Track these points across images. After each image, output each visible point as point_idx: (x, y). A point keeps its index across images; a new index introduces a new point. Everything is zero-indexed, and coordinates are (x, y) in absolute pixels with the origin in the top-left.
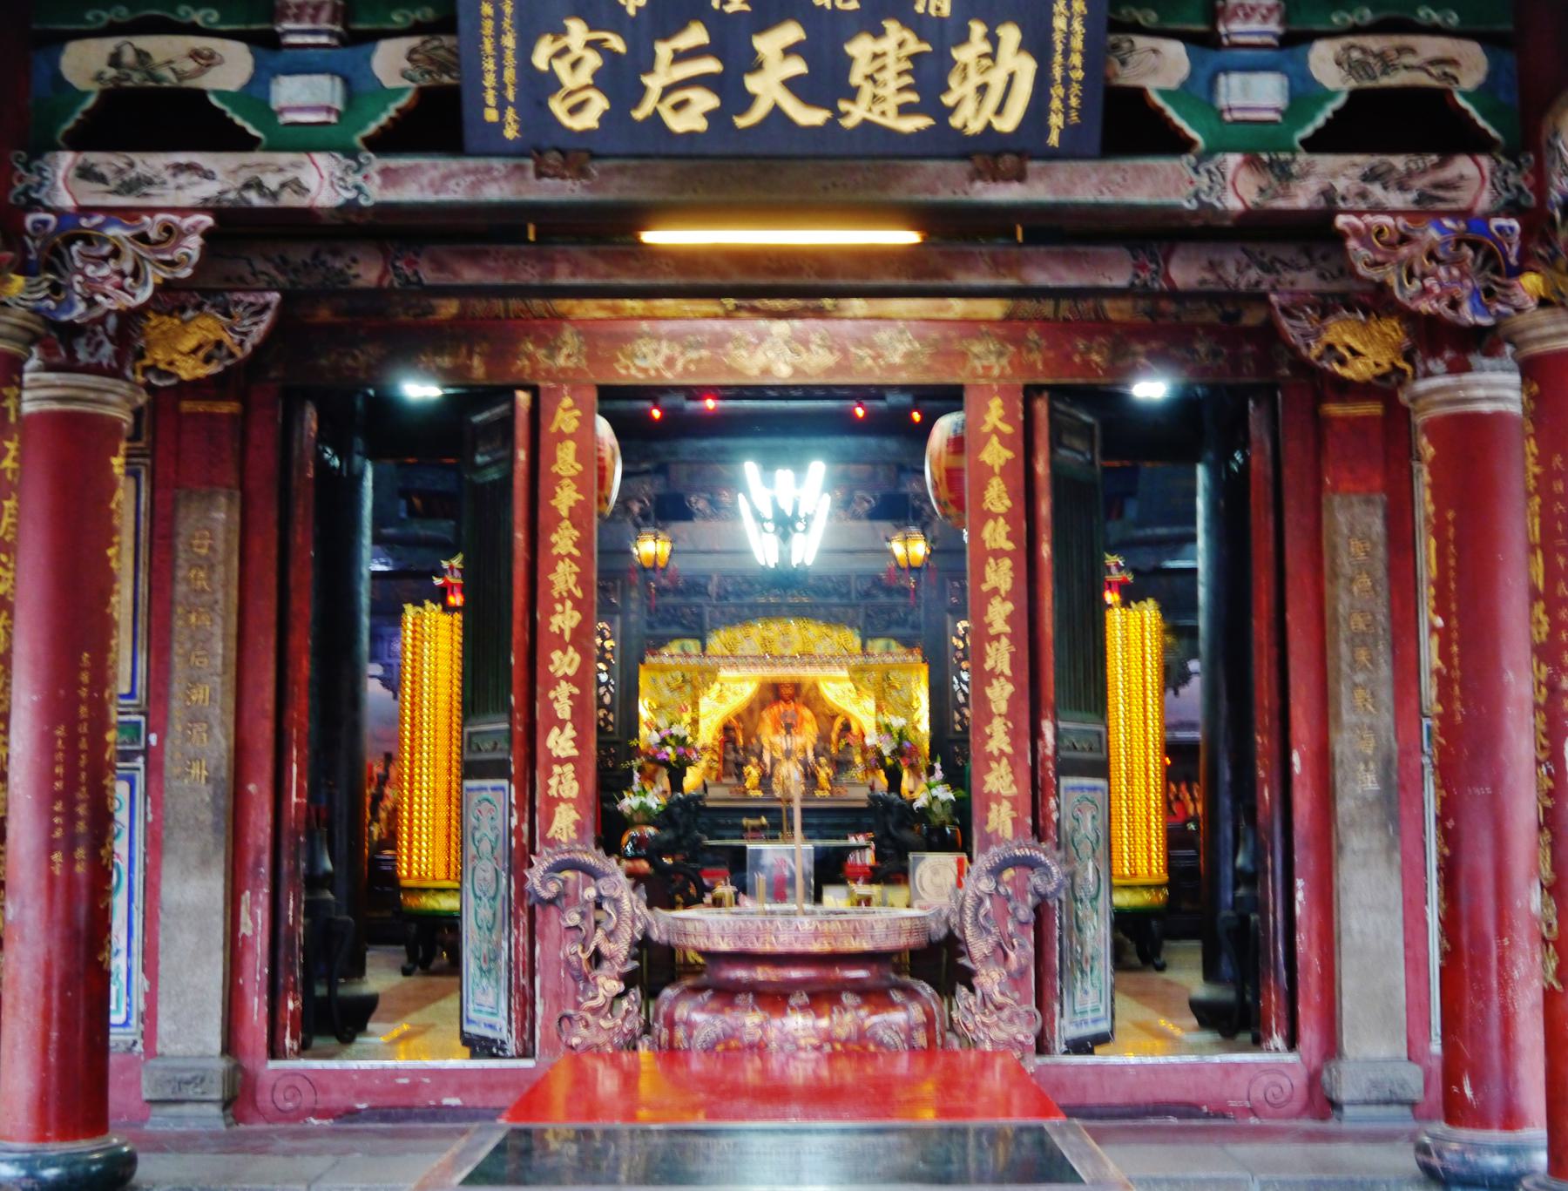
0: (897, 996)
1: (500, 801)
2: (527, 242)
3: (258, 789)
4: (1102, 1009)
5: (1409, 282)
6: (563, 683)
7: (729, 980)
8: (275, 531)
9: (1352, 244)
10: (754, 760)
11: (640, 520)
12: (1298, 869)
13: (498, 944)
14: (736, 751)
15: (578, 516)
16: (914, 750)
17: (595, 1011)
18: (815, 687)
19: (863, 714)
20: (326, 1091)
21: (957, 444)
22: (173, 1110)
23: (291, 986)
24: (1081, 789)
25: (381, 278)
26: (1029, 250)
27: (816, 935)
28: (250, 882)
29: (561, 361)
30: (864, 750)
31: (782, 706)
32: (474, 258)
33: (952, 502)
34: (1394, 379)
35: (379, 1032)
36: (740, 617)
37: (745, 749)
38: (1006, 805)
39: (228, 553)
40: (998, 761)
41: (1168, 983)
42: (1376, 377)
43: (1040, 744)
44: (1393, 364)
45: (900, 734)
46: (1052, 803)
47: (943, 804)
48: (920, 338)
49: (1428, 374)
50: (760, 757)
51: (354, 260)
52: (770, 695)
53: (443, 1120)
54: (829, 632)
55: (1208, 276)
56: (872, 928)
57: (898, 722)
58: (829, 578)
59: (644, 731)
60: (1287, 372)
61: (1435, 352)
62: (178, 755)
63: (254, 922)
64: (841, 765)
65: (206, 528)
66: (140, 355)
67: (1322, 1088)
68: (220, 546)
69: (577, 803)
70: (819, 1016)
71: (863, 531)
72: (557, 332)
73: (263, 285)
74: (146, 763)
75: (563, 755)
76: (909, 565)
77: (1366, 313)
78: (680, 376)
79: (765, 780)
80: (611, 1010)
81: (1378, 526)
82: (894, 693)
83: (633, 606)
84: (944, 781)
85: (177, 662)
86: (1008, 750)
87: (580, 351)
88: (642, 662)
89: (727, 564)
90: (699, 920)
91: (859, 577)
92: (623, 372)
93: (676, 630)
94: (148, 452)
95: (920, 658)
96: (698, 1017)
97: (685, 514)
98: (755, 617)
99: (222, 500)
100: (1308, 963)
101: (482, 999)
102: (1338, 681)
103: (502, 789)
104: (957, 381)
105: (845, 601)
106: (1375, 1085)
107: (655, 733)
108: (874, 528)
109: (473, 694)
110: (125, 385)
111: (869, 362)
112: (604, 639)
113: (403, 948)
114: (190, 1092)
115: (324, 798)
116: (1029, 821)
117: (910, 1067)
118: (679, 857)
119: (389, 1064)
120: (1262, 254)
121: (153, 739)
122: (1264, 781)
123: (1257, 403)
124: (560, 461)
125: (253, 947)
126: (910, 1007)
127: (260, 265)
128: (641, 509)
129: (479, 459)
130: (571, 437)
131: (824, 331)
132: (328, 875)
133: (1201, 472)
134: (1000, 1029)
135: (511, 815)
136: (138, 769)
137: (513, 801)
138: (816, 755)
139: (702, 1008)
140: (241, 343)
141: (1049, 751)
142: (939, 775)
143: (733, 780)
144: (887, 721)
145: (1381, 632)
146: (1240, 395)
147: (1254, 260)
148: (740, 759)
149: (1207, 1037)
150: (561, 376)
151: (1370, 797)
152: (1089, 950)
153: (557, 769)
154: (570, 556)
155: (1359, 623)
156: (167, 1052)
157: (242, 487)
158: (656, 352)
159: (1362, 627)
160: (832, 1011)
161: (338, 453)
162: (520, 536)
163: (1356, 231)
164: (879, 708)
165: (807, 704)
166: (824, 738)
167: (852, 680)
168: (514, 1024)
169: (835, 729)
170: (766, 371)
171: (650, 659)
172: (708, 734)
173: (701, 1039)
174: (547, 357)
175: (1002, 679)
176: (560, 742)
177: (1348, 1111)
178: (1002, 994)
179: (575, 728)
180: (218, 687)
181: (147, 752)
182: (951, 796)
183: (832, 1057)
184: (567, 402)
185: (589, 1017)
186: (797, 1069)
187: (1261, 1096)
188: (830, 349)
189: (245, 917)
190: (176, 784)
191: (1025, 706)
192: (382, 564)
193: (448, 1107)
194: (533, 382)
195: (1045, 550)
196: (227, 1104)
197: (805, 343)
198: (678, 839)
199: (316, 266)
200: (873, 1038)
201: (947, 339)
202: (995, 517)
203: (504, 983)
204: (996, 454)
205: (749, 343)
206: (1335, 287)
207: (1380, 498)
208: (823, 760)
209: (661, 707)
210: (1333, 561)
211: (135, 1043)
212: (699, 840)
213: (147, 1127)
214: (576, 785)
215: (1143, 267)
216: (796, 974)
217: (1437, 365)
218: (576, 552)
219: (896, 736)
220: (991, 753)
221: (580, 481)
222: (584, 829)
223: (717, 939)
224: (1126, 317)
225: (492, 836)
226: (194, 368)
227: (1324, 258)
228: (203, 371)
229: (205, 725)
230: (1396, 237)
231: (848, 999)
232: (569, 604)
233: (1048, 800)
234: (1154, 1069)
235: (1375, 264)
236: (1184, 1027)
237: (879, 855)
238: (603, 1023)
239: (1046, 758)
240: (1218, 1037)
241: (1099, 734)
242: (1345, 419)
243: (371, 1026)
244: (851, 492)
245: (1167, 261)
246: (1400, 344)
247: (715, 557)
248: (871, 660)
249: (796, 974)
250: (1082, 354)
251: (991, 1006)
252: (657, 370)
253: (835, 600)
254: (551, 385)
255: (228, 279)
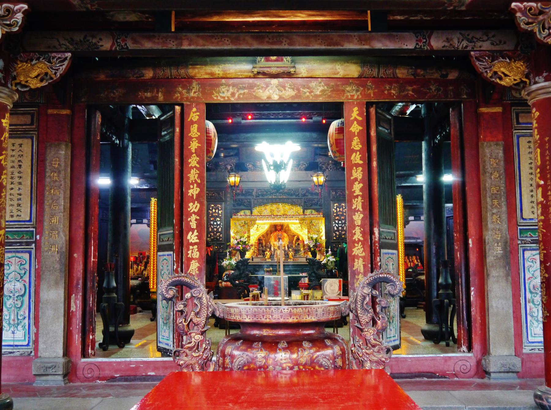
0: (328, 342)
1: (170, 259)
2: (171, 32)
3: (78, 256)
4: (397, 335)
5: (544, 31)
6: (193, 215)
7: (250, 335)
8: (84, 159)
9: (518, 14)
10: (268, 250)
11: (230, 171)
12: (471, 283)
13: (170, 313)
14: (262, 247)
15: (198, 152)
16: (321, 245)
17: (190, 349)
18: (288, 226)
19: (304, 234)
20: (103, 370)
21: (340, 130)
22: (44, 378)
23: (91, 330)
24: (389, 254)
25: (111, 47)
26: (373, 34)
27: (291, 315)
28: (75, 291)
29: (192, 94)
30: (304, 246)
31: (277, 232)
32: (149, 38)
33: (337, 151)
34: (522, 85)
35: (135, 343)
36: (263, 203)
37: (265, 246)
38: (361, 260)
39: (66, 166)
40: (358, 244)
41: (407, 322)
42: (515, 85)
43: (373, 237)
44: (520, 79)
45: (316, 240)
46: (378, 259)
47: (331, 262)
48: (327, 85)
49: (536, 83)
50: (270, 248)
51: (101, 39)
52: (273, 229)
53: (148, 381)
54: (292, 207)
55: (446, 44)
56: (317, 311)
57: (315, 236)
58: (292, 190)
59: (232, 240)
60: (465, 96)
61: (539, 74)
62: (47, 243)
63: (76, 306)
64: (297, 251)
65: (57, 157)
66: (14, 78)
67: (483, 366)
68: (63, 165)
69: (199, 260)
70: (292, 353)
71: (303, 174)
72: (191, 83)
73: (63, 49)
74: (35, 246)
75: (193, 242)
76: (319, 185)
77: (510, 59)
78: (237, 100)
79: (272, 256)
80: (198, 348)
81: (501, 154)
82: (314, 227)
83: (228, 199)
84: (332, 255)
85: (47, 208)
86: (361, 239)
87: (199, 91)
88: (231, 217)
89: (259, 185)
90: (236, 307)
91: (302, 189)
92: (215, 98)
93: (242, 207)
94: (36, 129)
95: (322, 216)
96: (236, 353)
97: (245, 169)
98: (268, 203)
99: (63, 147)
100: (476, 319)
101: (164, 334)
102: (486, 212)
103: (171, 255)
104: (341, 101)
105: (297, 197)
106: (503, 365)
107: (235, 240)
108: (307, 173)
109: (161, 220)
110: (7, 90)
111: (308, 94)
112: (219, 210)
113: (151, 311)
114: (50, 371)
115: (114, 261)
116: (370, 265)
117: (334, 374)
118: (240, 281)
119: (128, 359)
120: (468, 35)
121: (38, 237)
122: (457, 250)
123: (453, 110)
124: (192, 132)
125: (76, 316)
126: (334, 348)
127: (62, 42)
128: (231, 168)
129: (163, 133)
130: (196, 122)
131: (290, 82)
132: (114, 288)
133: (424, 144)
134: (374, 356)
135: (174, 265)
136: (33, 248)
137: (175, 259)
138: (288, 248)
139: (238, 349)
140: (55, 73)
141: (377, 240)
142: (330, 252)
143: (262, 256)
144: (311, 236)
145: (502, 193)
146: (449, 105)
147: (465, 38)
148: (264, 250)
149: (428, 344)
150: (192, 100)
151: (499, 256)
152: (392, 314)
153: (191, 247)
154: (195, 167)
155: (494, 190)
156: (42, 356)
157: (72, 141)
158: (228, 91)
159: (495, 192)
160: (299, 351)
161: (118, 138)
162: (177, 160)
163: (520, 9)
164: (309, 232)
165: (285, 232)
166: (291, 242)
167: (300, 223)
168: (175, 344)
169: (295, 240)
170: (269, 98)
171: (234, 217)
172: (253, 240)
173: (237, 363)
174: (187, 93)
175: (359, 213)
176: (192, 237)
177: (493, 375)
178: (375, 339)
179: (197, 232)
180: (62, 217)
181: (36, 242)
182: (334, 260)
183: (299, 372)
184: (194, 109)
185: (187, 351)
186: (282, 377)
187: (459, 369)
188: (293, 89)
189: (73, 304)
190: (46, 254)
191: (367, 222)
192: (146, 186)
193: (150, 375)
194: (182, 102)
195: (375, 164)
196: (65, 376)
197: (284, 87)
198: (240, 274)
199: (85, 42)
200: (317, 363)
201: (337, 86)
202: (356, 151)
203: (171, 328)
204: (356, 128)
205: (262, 87)
206: (497, 48)
207: (501, 143)
208: (290, 249)
209: (237, 232)
210: (484, 167)
211: (31, 352)
212: (248, 275)
213: (34, 385)
214: (198, 253)
215: (420, 41)
216: (281, 332)
217: (541, 79)
218: (198, 166)
219: (314, 241)
220: (355, 240)
221: (199, 139)
222: (201, 269)
223: (245, 316)
224: (404, 77)
225: (167, 273)
226: (36, 84)
227: (493, 36)
228: (39, 85)
229: (57, 232)
230: (537, 12)
231: (306, 344)
232: (195, 185)
233: (377, 258)
234: (418, 359)
235: (528, 24)
236: (419, 340)
237: (310, 280)
238: (193, 354)
239: (375, 242)
240: (433, 343)
241: (394, 234)
242: (488, 113)
243: (132, 341)
244: (299, 161)
245: (430, 38)
246: (524, 71)
247: (255, 183)
248: (306, 216)
249: (281, 332)
250: (388, 90)
251: (369, 345)
252: (228, 97)
253: (294, 197)
254: (189, 103)
255: (49, 47)
